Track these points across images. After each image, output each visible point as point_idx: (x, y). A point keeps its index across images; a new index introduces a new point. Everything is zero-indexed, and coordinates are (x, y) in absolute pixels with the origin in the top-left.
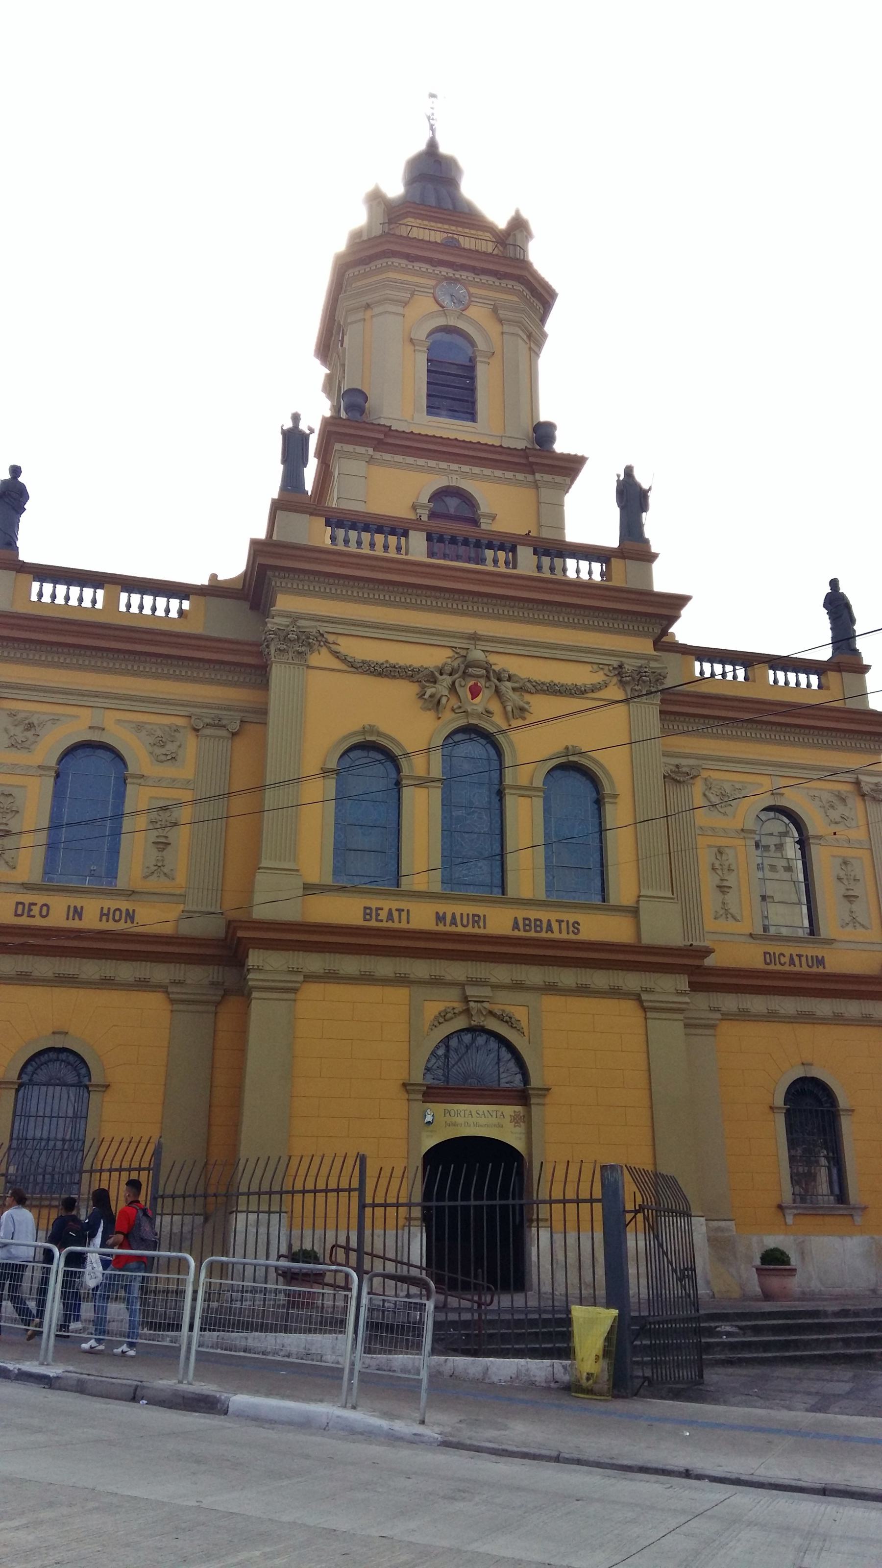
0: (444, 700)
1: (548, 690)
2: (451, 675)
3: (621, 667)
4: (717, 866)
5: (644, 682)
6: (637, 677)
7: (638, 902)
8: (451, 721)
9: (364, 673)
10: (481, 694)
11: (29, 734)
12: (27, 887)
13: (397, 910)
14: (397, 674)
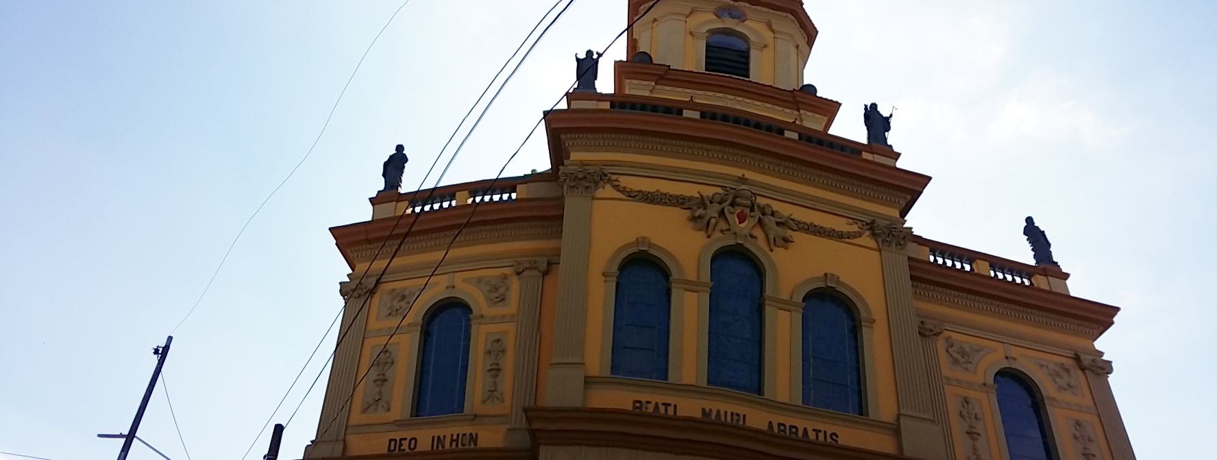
0: (713, 221)
1: (808, 229)
2: (720, 203)
3: (873, 222)
4: (964, 413)
5: (894, 236)
6: (887, 232)
7: (898, 420)
8: (720, 241)
9: (640, 200)
10: (747, 221)
11: (403, 303)
12: (399, 424)
13: (663, 404)
14: (667, 201)
